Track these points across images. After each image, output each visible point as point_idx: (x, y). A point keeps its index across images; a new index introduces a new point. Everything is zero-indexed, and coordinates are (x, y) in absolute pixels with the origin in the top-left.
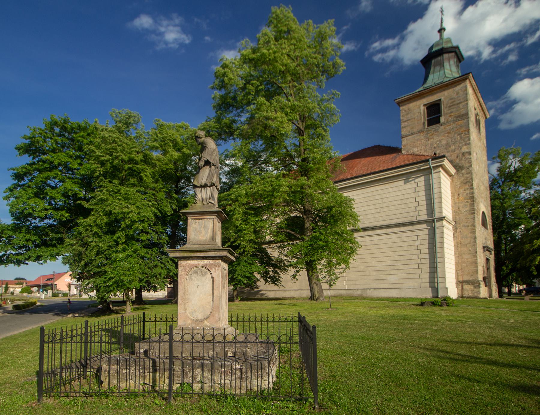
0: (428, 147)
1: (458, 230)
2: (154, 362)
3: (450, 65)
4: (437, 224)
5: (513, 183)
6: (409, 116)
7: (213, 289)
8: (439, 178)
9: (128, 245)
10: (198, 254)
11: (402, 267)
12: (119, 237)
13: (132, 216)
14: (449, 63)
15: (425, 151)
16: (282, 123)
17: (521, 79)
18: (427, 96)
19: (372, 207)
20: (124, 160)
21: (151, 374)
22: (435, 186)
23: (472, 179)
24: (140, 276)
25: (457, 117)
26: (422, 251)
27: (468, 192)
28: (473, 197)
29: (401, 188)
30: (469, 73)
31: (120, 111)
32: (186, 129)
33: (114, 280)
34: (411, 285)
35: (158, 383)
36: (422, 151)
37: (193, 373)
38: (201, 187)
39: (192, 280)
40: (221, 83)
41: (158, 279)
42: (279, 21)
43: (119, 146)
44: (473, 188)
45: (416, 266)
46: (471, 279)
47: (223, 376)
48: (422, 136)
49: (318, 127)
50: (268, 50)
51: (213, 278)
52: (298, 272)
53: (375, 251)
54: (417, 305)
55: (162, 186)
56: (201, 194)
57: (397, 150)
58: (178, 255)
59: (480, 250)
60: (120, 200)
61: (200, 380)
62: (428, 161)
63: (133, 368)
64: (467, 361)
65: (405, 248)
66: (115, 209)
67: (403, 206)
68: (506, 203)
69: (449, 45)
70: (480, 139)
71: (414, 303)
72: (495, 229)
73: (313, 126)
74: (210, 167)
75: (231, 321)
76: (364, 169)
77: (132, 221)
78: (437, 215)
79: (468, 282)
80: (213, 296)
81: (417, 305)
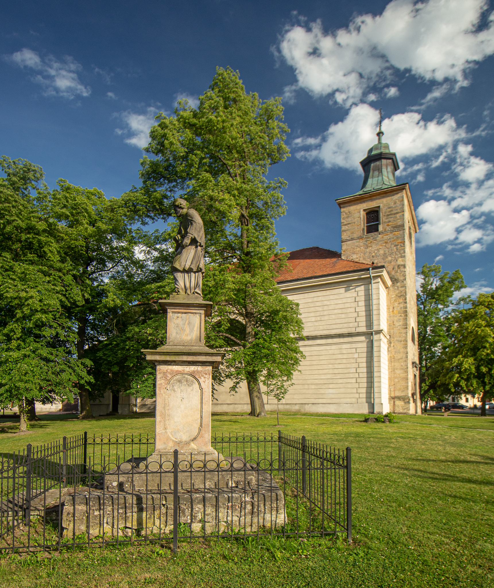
1: (392, 345)
2: (139, 500)
4: (375, 337)
5: (434, 300)
7: (202, 403)
8: (378, 288)
9: (24, 341)
10: (185, 358)
11: (340, 381)
12: (12, 331)
13: (33, 303)
15: (364, 259)
16: (230, 206)
17: (428, 200)
18: (367, 201)
19: (312, 314)
20: (21, 228)
21: (135, 515)
22: (374, 297)
23: (406, 293)
24: (41, 383)
25: (394, 227)
26: (361, 365)
27: (402, 305)
28: (406, 311)
29: (341, 296)
31: (16, 161)
32: (99, 198)
33: (7, 387)
34: (349, 400)
35: (144, 526)
37: (192, 511)
38: (184, 271)
39: (174, 391)
40: (159, 147)
41: (65, 388)
42: (226, 86)
43: (13, 207)
44: (406, 303)
45: (354, 380)
46: (402, 395)
47: (230, 512)
48: (361, 243)
49: (263, 218)
50: (216, 117)
51: (201, 389)
52: (238, 383)
53: (314, 363)
54: (361, 421)
55: (71, 268)
56: (182, 280)
57: (336, 255)
58: (158, 358)
59: (410, 366)
60: (14, 280)
61: (202, 519)
62: (368, 270)
63: (110, 508)
64: (446, 480)
65: (344, 361)
66: (7, 292)
67: (343, 316)
68: (428, 319)
69: (387, 151)
70: (411, 253)
71: (356, 419)
72: (420, 345)
73: (258, 216)
74: (197, 247)
75: (215, 441)
76: (305, 271)
77: (31, 310)
78: (375, 328)
79: (399, 398)
80: (202, 412)
81: (361, 421)
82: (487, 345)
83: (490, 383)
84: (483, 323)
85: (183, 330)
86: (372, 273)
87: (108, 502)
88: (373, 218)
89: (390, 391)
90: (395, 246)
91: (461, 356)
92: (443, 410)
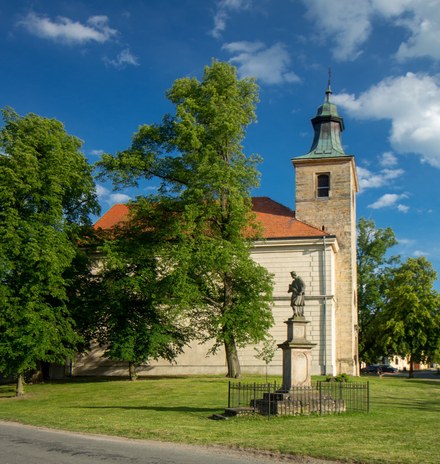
0: (318, 218)
1: (339, 308)
3: (335, 135)
6: (303, 180)
7: (307, 365)
14: (335, 132)
23: (351, 259)
27: (347, 271)
30: (352, 156)
36: (313, 221)
38: (298, 306)
44: (351, 269)
48: (313, 205)
51: (307, 359)
57: (292, 214)
62: (322, 237)
78: (327, 294)
80: (307, 369)
82: (414, 310)
83: (416, 346)
84: (411, 288)
85: (298, 333)
86: (326, 241)
87: (291, 403)
88: (324, 180)
89: (337, 353)
90: (343, 213)
91: (393, 319)
92: (378, 373)
